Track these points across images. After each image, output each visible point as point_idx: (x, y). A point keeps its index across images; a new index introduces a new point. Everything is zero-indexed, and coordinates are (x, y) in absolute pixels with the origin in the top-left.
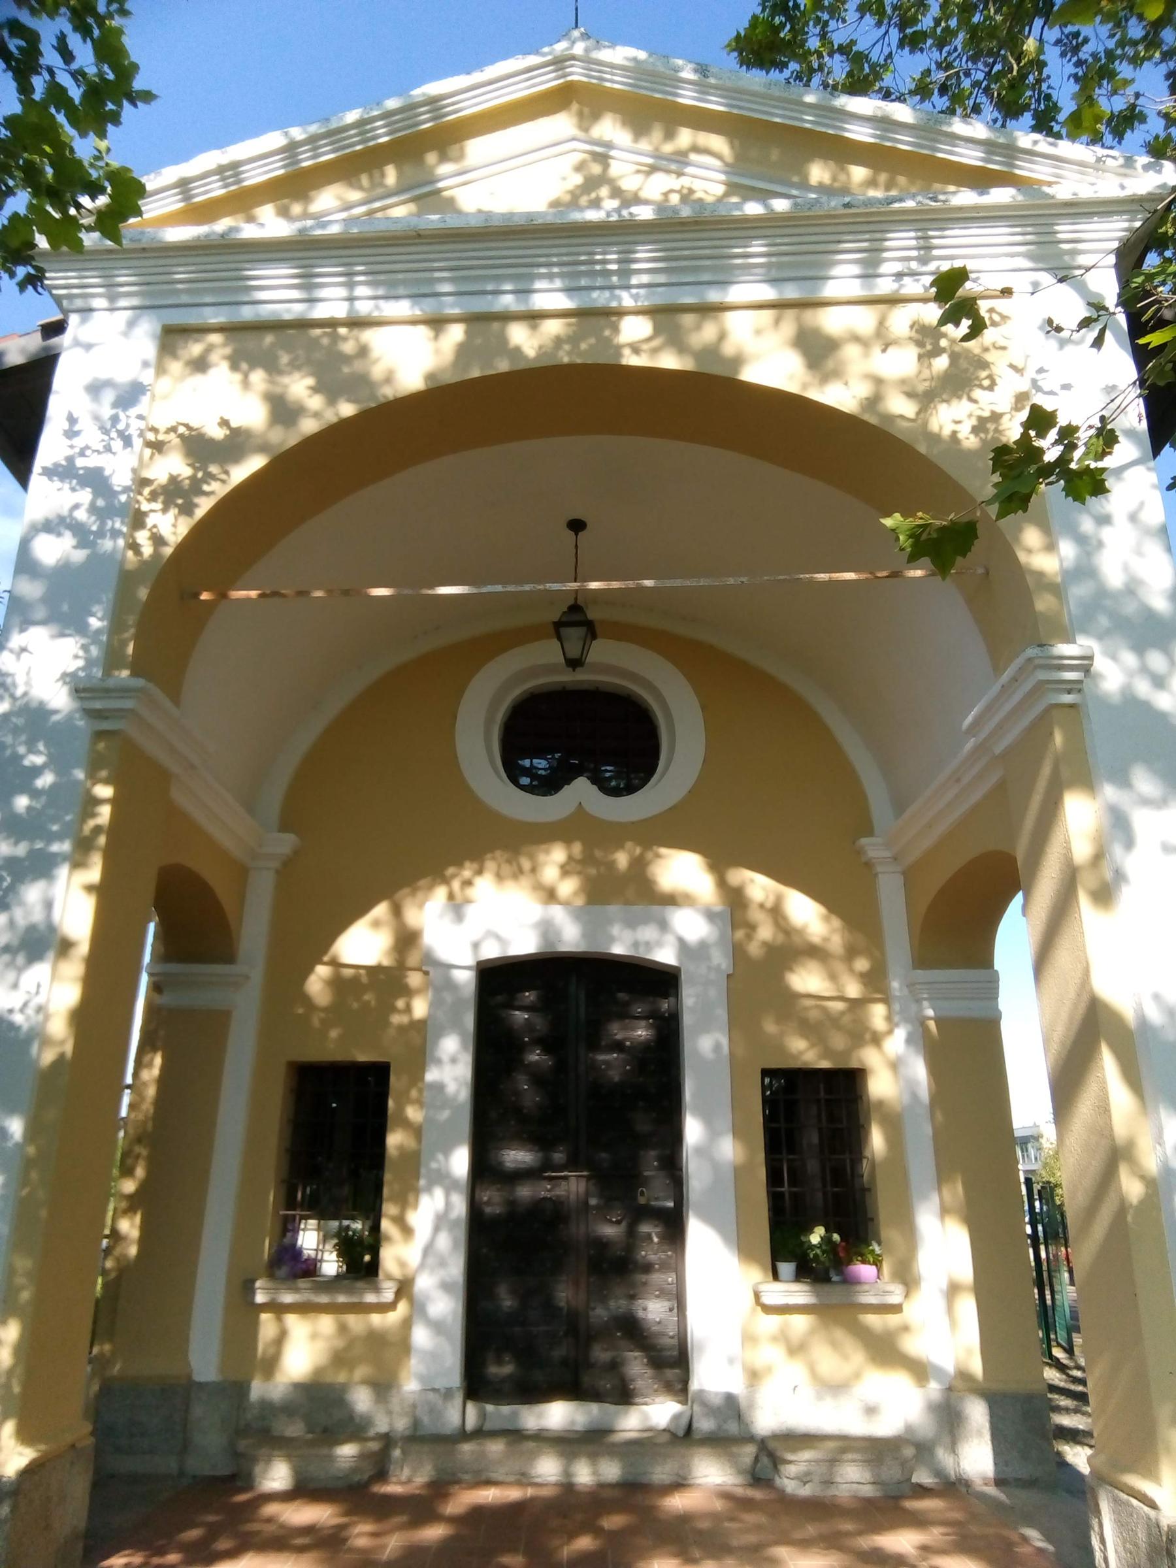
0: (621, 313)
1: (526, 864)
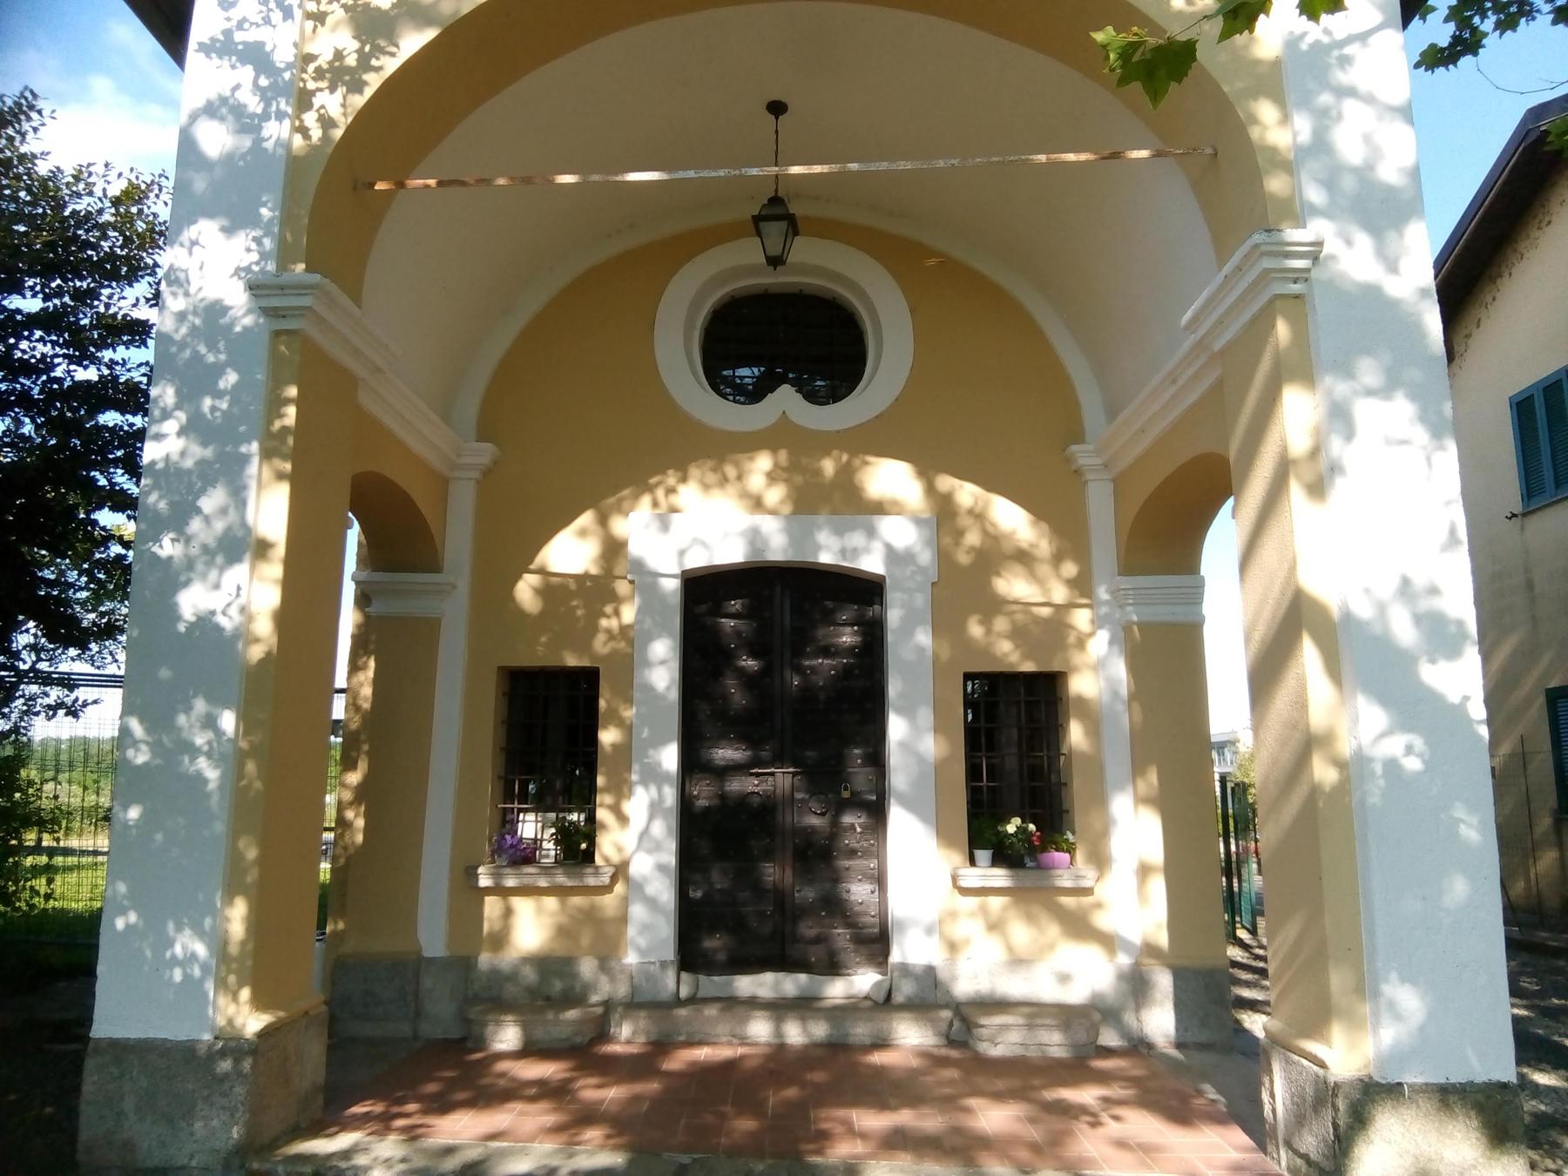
1: (730, 471)
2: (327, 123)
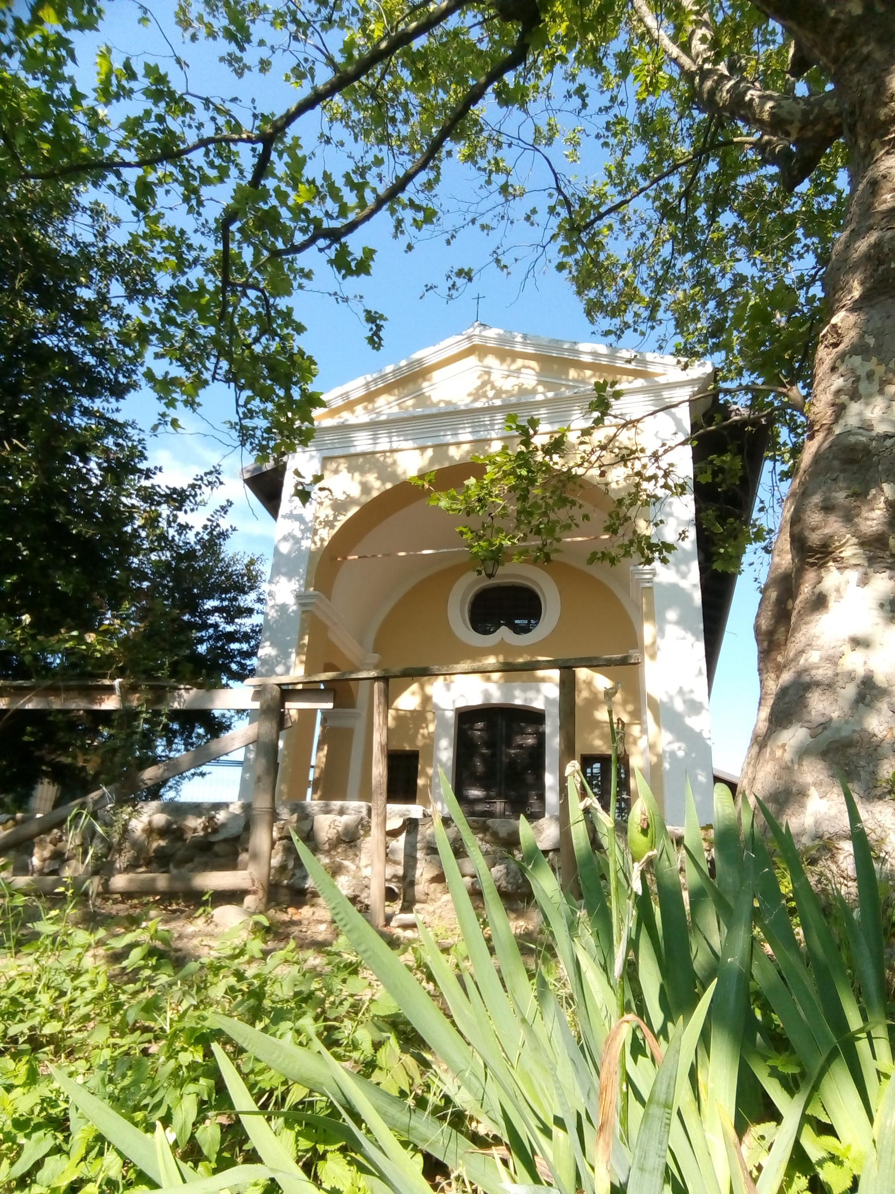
0: (491, 440)
2: (322, 540)
